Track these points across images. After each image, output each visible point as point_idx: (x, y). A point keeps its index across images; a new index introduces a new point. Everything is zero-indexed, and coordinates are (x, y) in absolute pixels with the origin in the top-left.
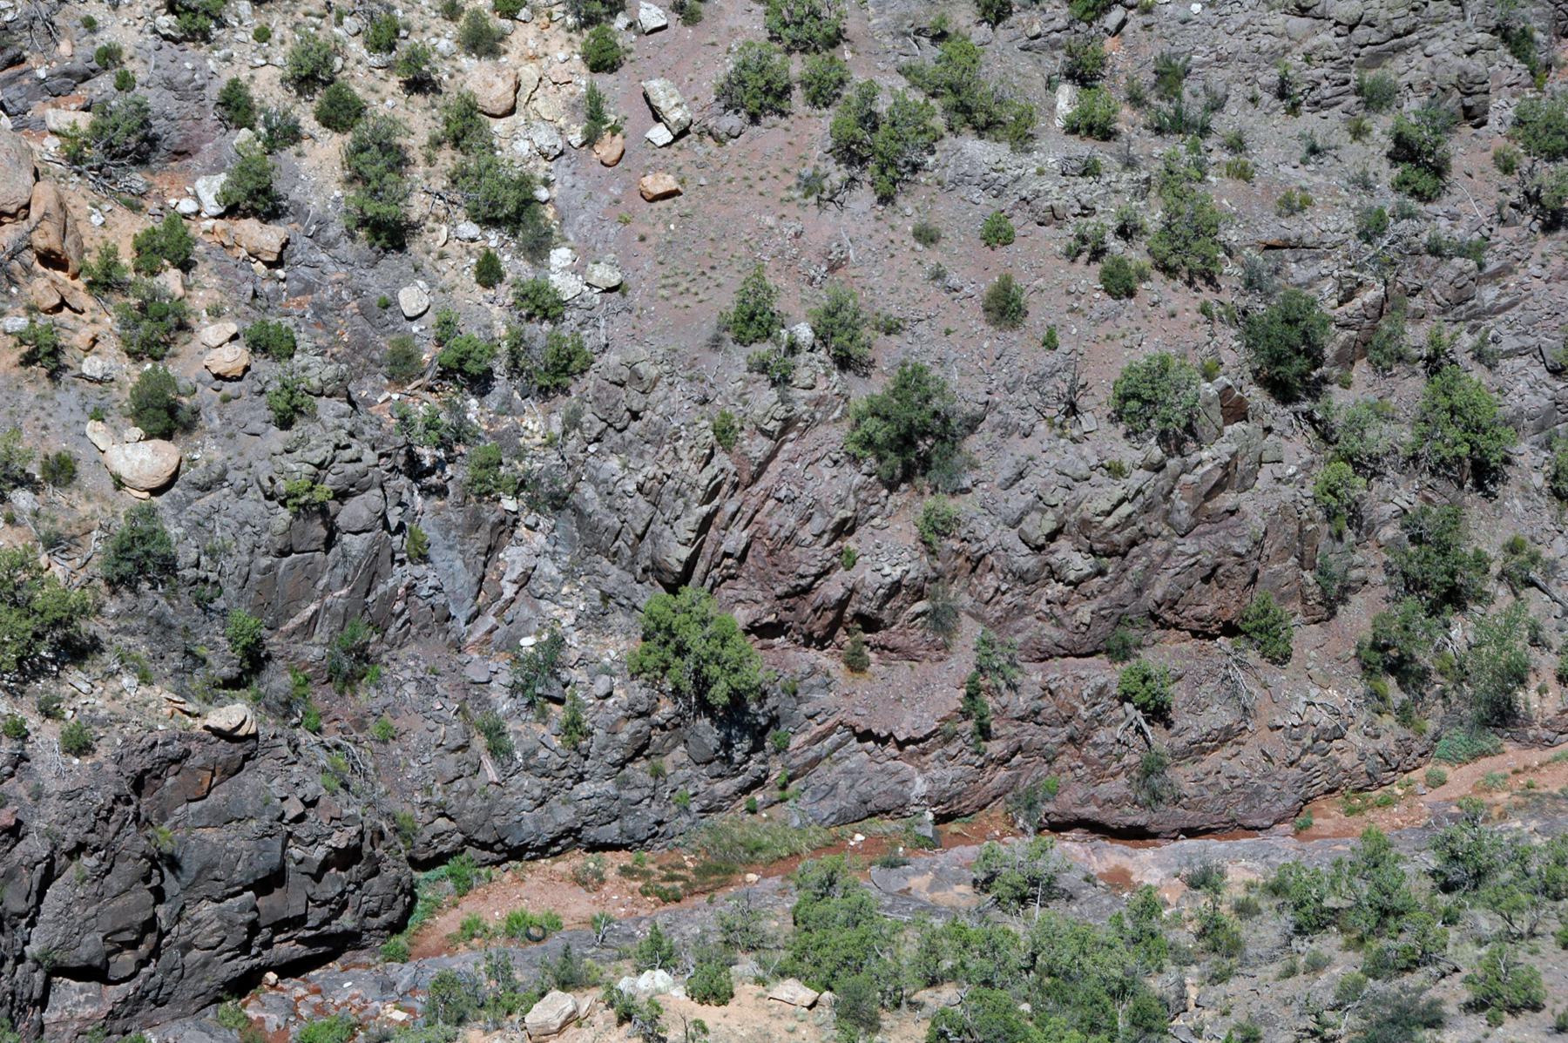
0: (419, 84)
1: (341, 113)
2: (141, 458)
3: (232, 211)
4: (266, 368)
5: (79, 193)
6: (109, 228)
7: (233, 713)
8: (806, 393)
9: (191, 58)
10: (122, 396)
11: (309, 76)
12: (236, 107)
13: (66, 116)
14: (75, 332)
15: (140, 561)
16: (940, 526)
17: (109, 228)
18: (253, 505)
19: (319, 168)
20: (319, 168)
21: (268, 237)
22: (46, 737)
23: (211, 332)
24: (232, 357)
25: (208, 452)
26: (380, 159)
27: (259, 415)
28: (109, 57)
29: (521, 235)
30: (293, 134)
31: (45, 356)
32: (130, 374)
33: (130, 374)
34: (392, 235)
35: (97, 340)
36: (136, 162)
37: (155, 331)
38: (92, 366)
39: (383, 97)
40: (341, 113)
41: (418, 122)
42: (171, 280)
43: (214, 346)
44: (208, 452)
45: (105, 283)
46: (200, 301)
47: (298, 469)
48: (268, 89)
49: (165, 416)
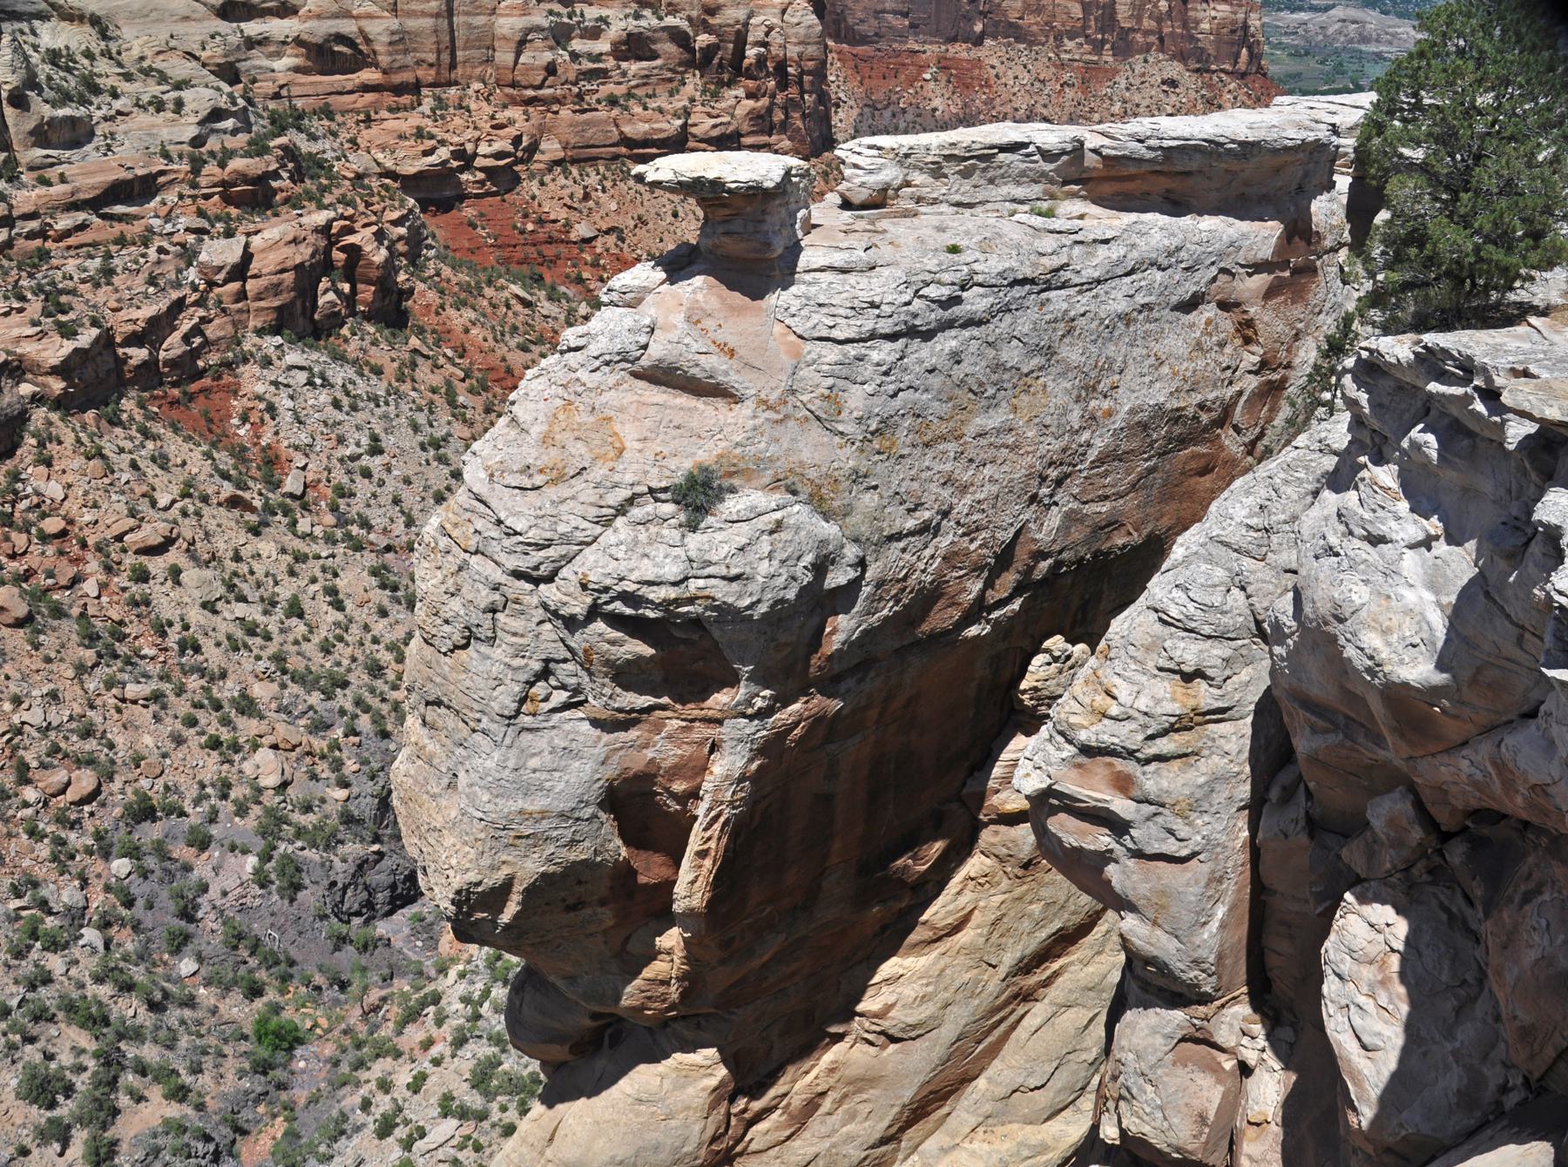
0: (384, 700)
1: (367, 709)
2: (341, 794)
3: (346, 736)
6: (319, 744)
7: (376, 847)
8: (423, 56)
9: (329, 704)
11: (358, 702)
12: (342, 712)
13: (302, 722)
14: (318, 769)
15: (348, 819)
17: (319, 744)
18: (369, 799)
19: (364, 723)
20: (364, 723)
21: (356, 739)
22: (336, 860)
23: (349, 763)
25: (355, 790)
26: (378, 719)
27: (365, 778)
28: (311, 708)
30: (357, 716)
31: (314, 777)
33: (333, 776)
35: (323, 769)
36: (114, 1117)
37: (337, 765)
38: (324, 775)
39: (374, 702)
40: (367, 709)
41: (385, 708)
42: (337, 753)
43: (351, 766)
44: (355, 790)
45: (323, 757)
47: (378, 788)
49: (344, 784)
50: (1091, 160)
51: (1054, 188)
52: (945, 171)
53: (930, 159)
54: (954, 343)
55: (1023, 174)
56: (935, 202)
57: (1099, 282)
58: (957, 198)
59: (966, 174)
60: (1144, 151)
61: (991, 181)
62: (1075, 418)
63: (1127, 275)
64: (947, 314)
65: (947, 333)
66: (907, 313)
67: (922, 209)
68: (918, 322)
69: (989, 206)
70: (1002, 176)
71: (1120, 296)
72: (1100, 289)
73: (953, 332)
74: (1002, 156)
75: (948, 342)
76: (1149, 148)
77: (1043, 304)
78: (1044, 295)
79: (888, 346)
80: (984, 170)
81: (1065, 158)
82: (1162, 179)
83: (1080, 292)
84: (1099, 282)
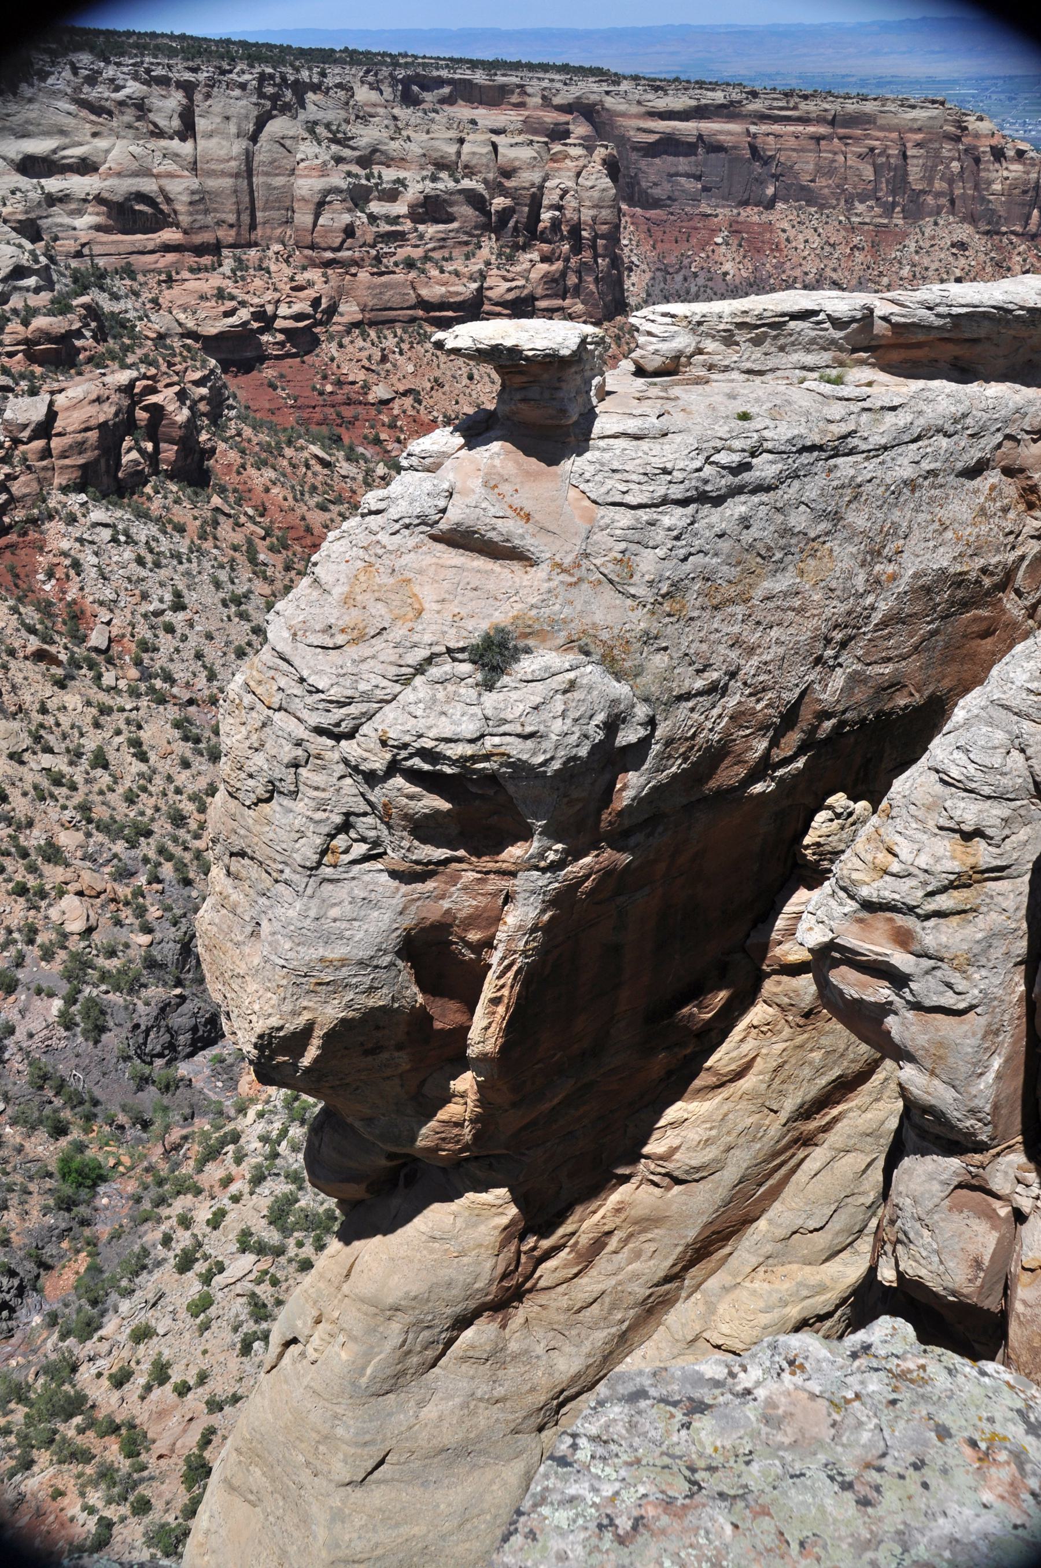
0: (186, 849)
1: (170, 858)
2: (145, 939)
3: (149, 883)
4: (168, 915)
5: (116, 886)
6: (123, 891)
7: (178, 991)
8: (223, 216)
10: (136, 927)
11: (161, 851)
12: (146, 860)
13: (107, 869)
14: (122, 915)
16: (469, 1526)
17: (123, 891)
18: (171, 945)
19: (167, 870)
20: (167, 870)
21: (160, 887)
22: (139, 1003)
23: (152, 909)
24: (159, 913)
25: (158, 935)
26: (180, 867)
27: (167, 925)
28: (115, 856)
29: (136, 1248)
32: (137, 922)
33: (137, 922)
34: (187, 882)
35: (127, 915)
37: (141, 912)
39: (177, 851)
40: (170, 858)
41: (188, 857)
43: (154, 912)
44: (158, 935)
45: (127, 904)
46: (148, 903)
47: (180, 933)
48: (152, 854)
49: (147, 930)
50: (880, 327)
51: (844, 356)
52: (737, 338)
53: (722, 327)
54: (743, 509)
55: (813, 341)
56: (726, 369)
57: (885, 448)
58: (748, 365)
59: (757, 342)
60: (933, 318)
61: (782, 349)
62: (860, 582)
63: (913, 441)
64: (737, 480)
65: (737, 499)
66: (698, 479)
67: (714, 377)
68: (708, 488)
69: (779, 373)
70: (793, 344)
71: (906, 462)
72: (886, 456)
73: (743, 498)
74: (792, 324)
75: (737, 507)
76: (938, 315)
77: (830, 471)
78: (832, 462)
79: (679, 511)
80: (775, 337)
81: (854, 325)
82: (950, 347)
83: (867, 459)
84: (885, 448)
